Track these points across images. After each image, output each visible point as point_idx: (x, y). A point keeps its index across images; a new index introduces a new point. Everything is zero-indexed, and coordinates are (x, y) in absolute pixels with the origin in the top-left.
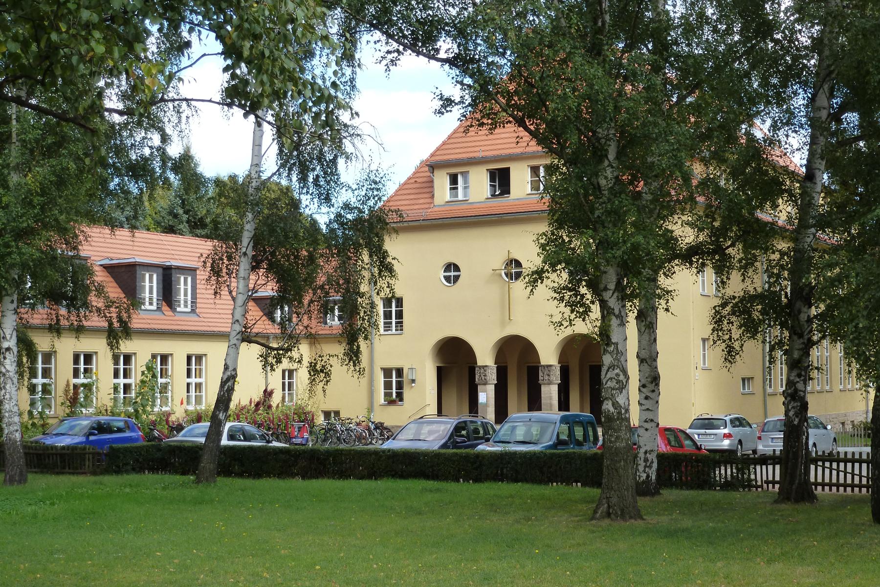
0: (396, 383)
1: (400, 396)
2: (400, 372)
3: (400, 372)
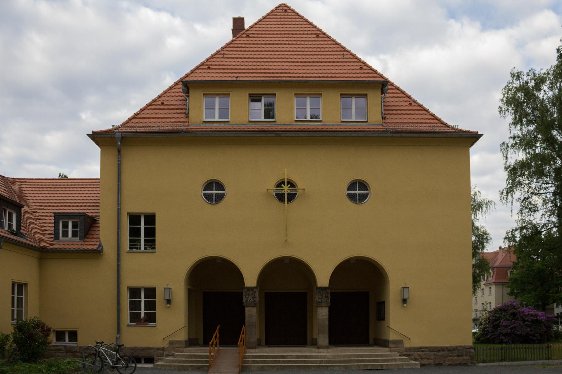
0: (143, 304)
1: (151, 318)
2: (151, 292)
3: (151, 292)
